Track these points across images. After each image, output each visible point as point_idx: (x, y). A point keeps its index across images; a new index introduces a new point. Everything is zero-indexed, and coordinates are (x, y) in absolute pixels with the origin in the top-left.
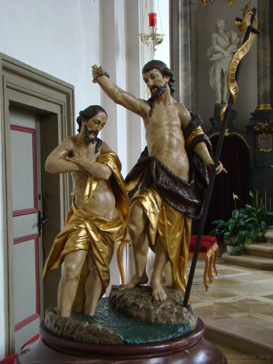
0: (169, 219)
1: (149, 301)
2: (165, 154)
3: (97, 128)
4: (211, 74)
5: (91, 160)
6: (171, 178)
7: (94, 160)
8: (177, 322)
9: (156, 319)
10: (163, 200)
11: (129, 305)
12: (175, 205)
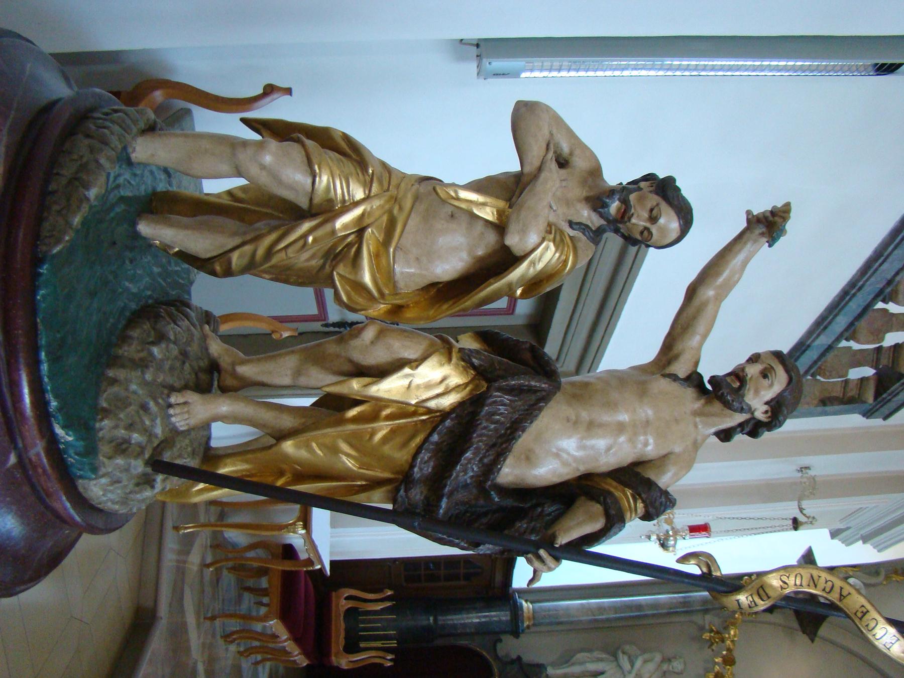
0: (393, 432)
1: (170, 380)
3: (638, 216)
5: (551, 207)
6: (509, 432)
7: (552, 218)
8: (103, 438)
9: (114, 381)
10: (444, 415)
11: (160, 325)
12: (432, 447)
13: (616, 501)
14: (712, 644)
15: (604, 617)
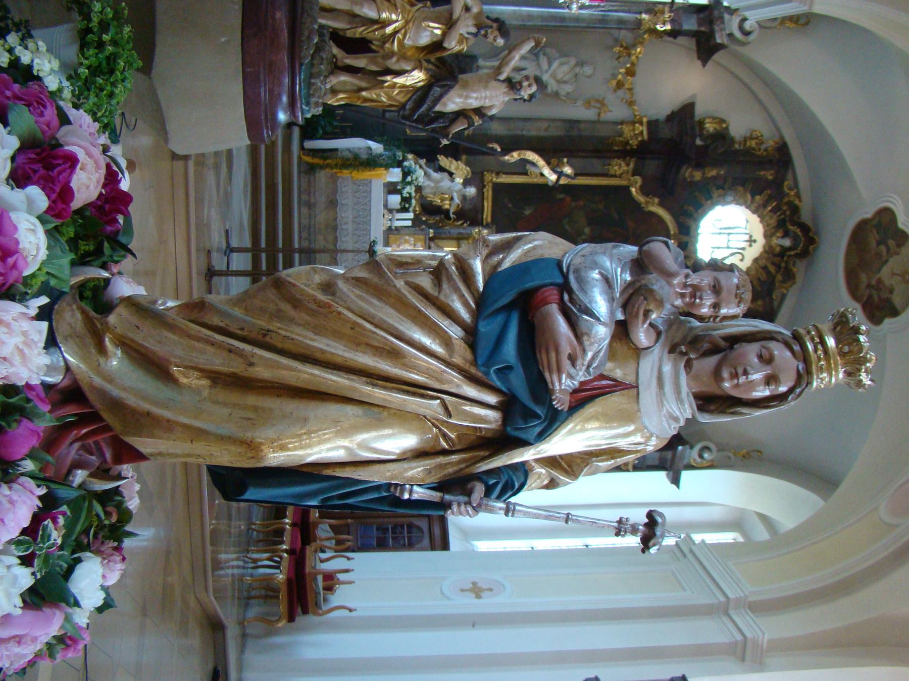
2: (460, 92)
9: (314, 84)
13: (472, 120)
14: (619, 57)
15: (531, 23)
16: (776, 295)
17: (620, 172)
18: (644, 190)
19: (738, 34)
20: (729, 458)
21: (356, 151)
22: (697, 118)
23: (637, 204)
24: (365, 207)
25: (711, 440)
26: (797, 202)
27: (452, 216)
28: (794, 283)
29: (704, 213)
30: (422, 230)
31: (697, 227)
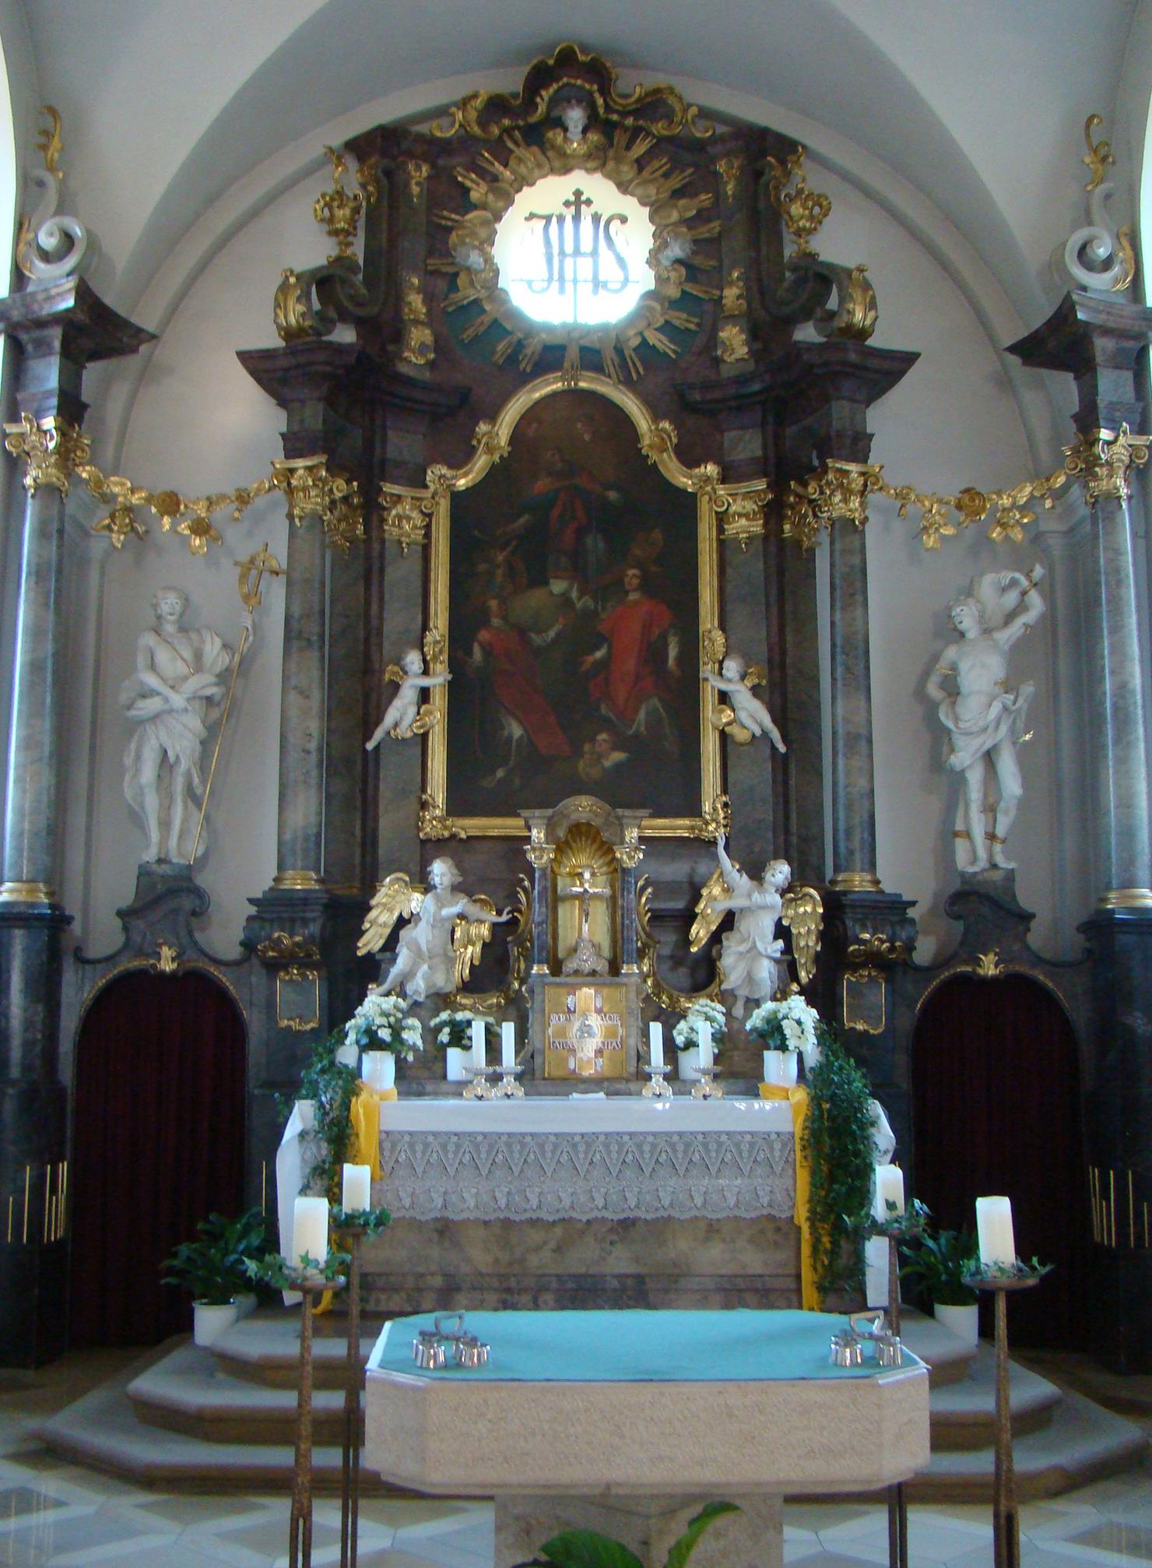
4: (128, 761)
16: (701, 132)
17: (418, 517)
18: (460, 459)
19: (71, 262)
20: (1108, 197)
21: (308, 1170)
22: (280, 343)
23: (494, 473)
24: (451, 1148)
25: (1064, 245)
26: (478, 103)
27: (504, 918)
28: (671, 90)
29: (515, 315)
30: (531, 991)
31: (549, 329)
